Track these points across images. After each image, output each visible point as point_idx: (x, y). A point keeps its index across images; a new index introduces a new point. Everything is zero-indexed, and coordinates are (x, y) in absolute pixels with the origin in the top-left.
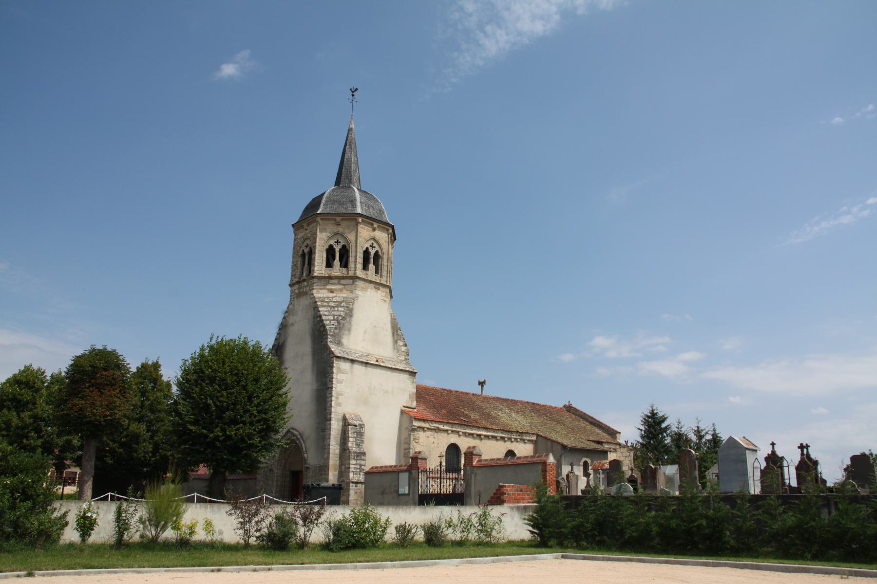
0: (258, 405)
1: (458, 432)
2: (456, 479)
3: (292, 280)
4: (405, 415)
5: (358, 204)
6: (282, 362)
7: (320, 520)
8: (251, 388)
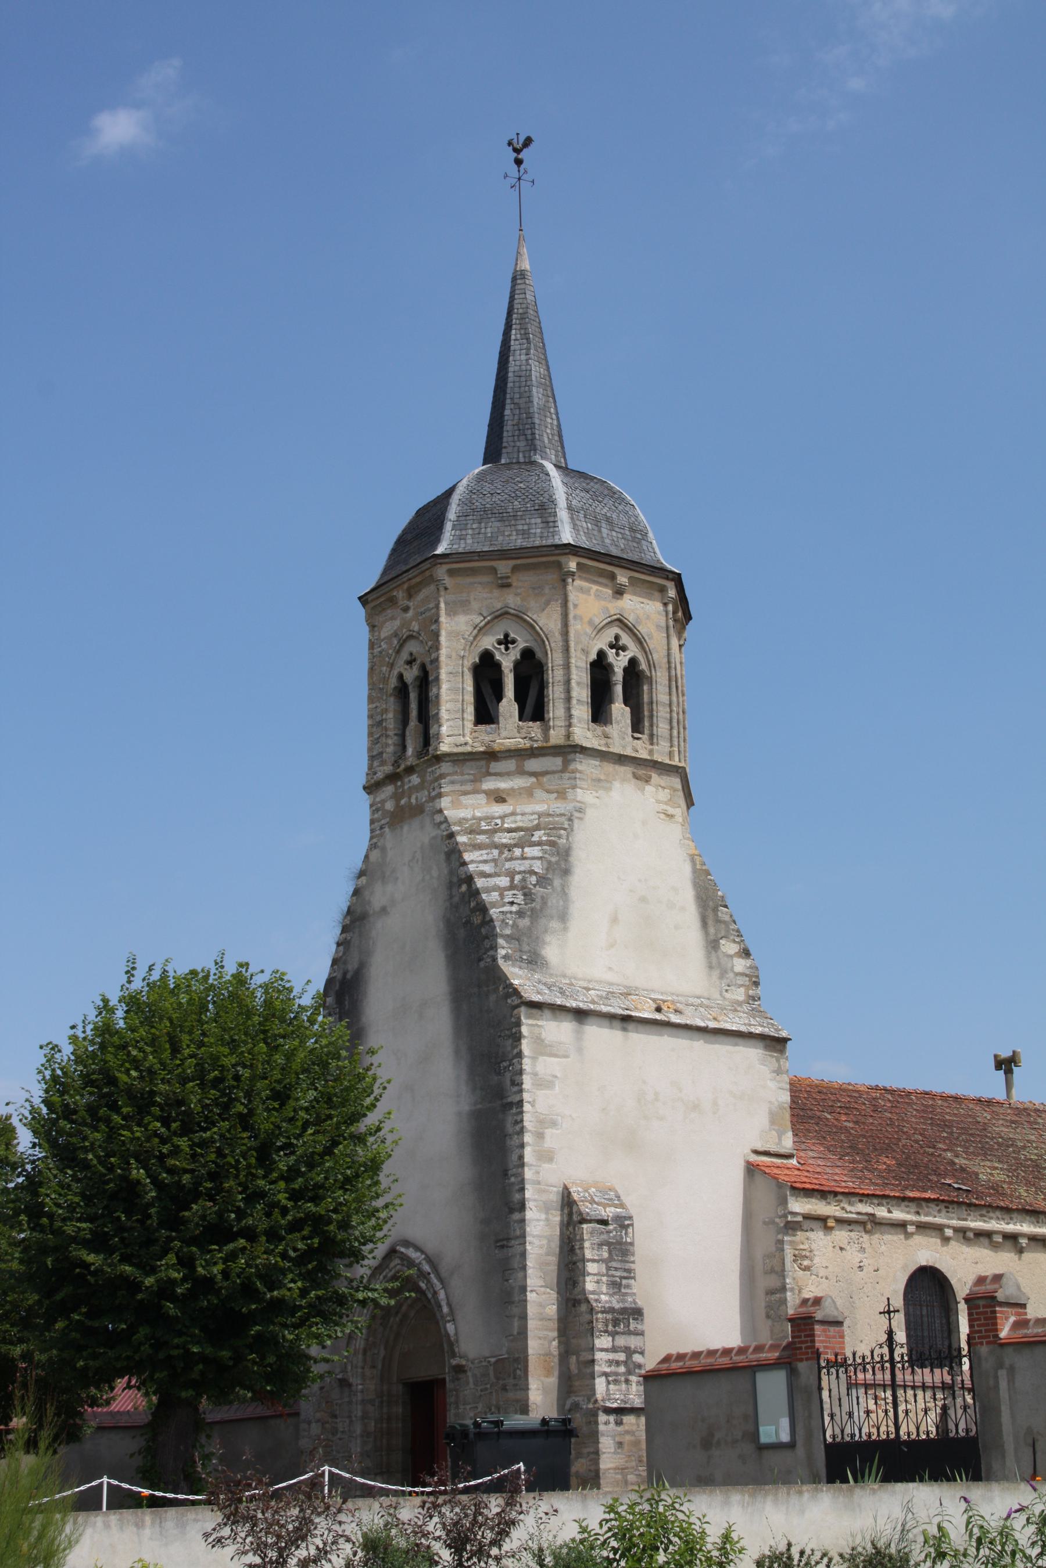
0: (292, 1174)
1: (939, 1229)
2: (944, 1387)
3: (371, 771)
4: (759, 1179)
5: (563, 515)
6: (357, 1034)
7: (507, 1546)
8: (264, 1121)
